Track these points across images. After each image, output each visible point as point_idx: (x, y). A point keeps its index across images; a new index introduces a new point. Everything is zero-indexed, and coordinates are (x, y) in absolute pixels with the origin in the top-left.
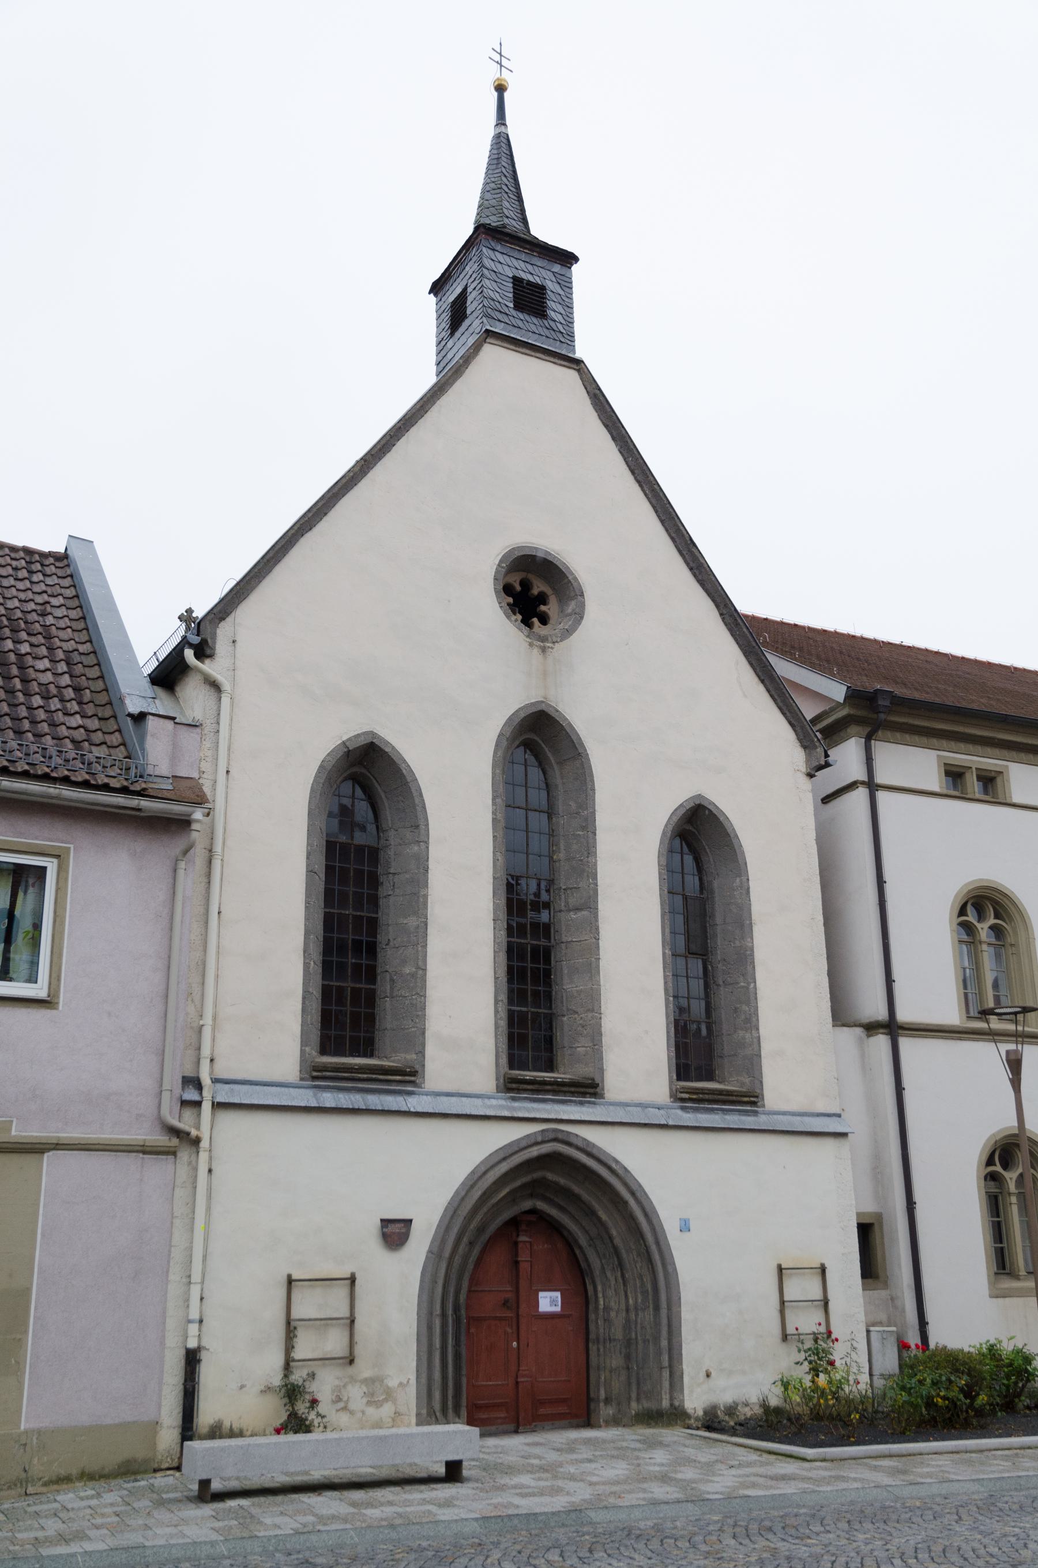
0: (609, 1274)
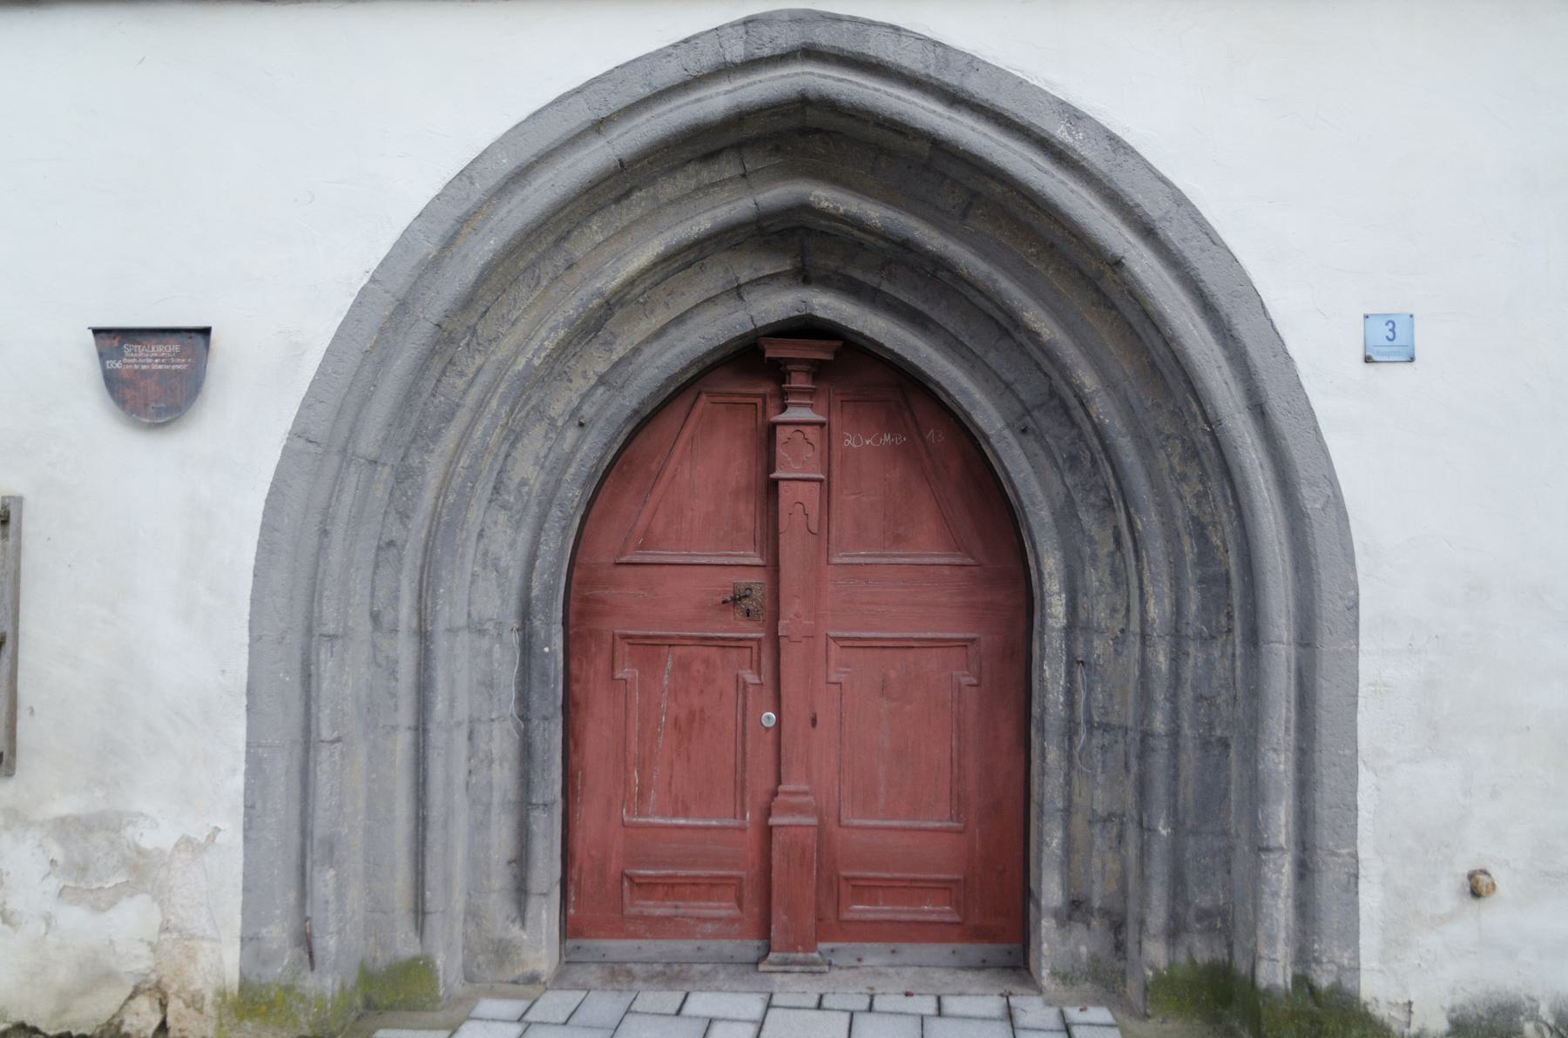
0: (1087, 518)
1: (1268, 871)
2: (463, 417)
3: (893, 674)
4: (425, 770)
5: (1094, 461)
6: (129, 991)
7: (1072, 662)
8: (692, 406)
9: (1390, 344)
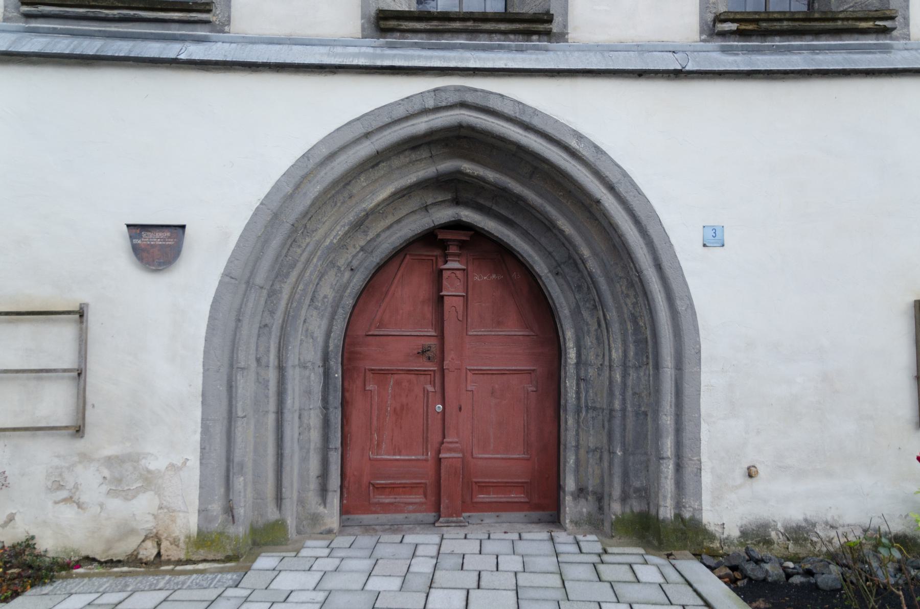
0: (586, 314)
1: (663, 468)
2: (300, 266)
3: (497, 386)
4: (282, 432)
5: (588, 288)
6: (143, 538)
7: (579, 379)
8: (403, 261)
9: (714, 239)
